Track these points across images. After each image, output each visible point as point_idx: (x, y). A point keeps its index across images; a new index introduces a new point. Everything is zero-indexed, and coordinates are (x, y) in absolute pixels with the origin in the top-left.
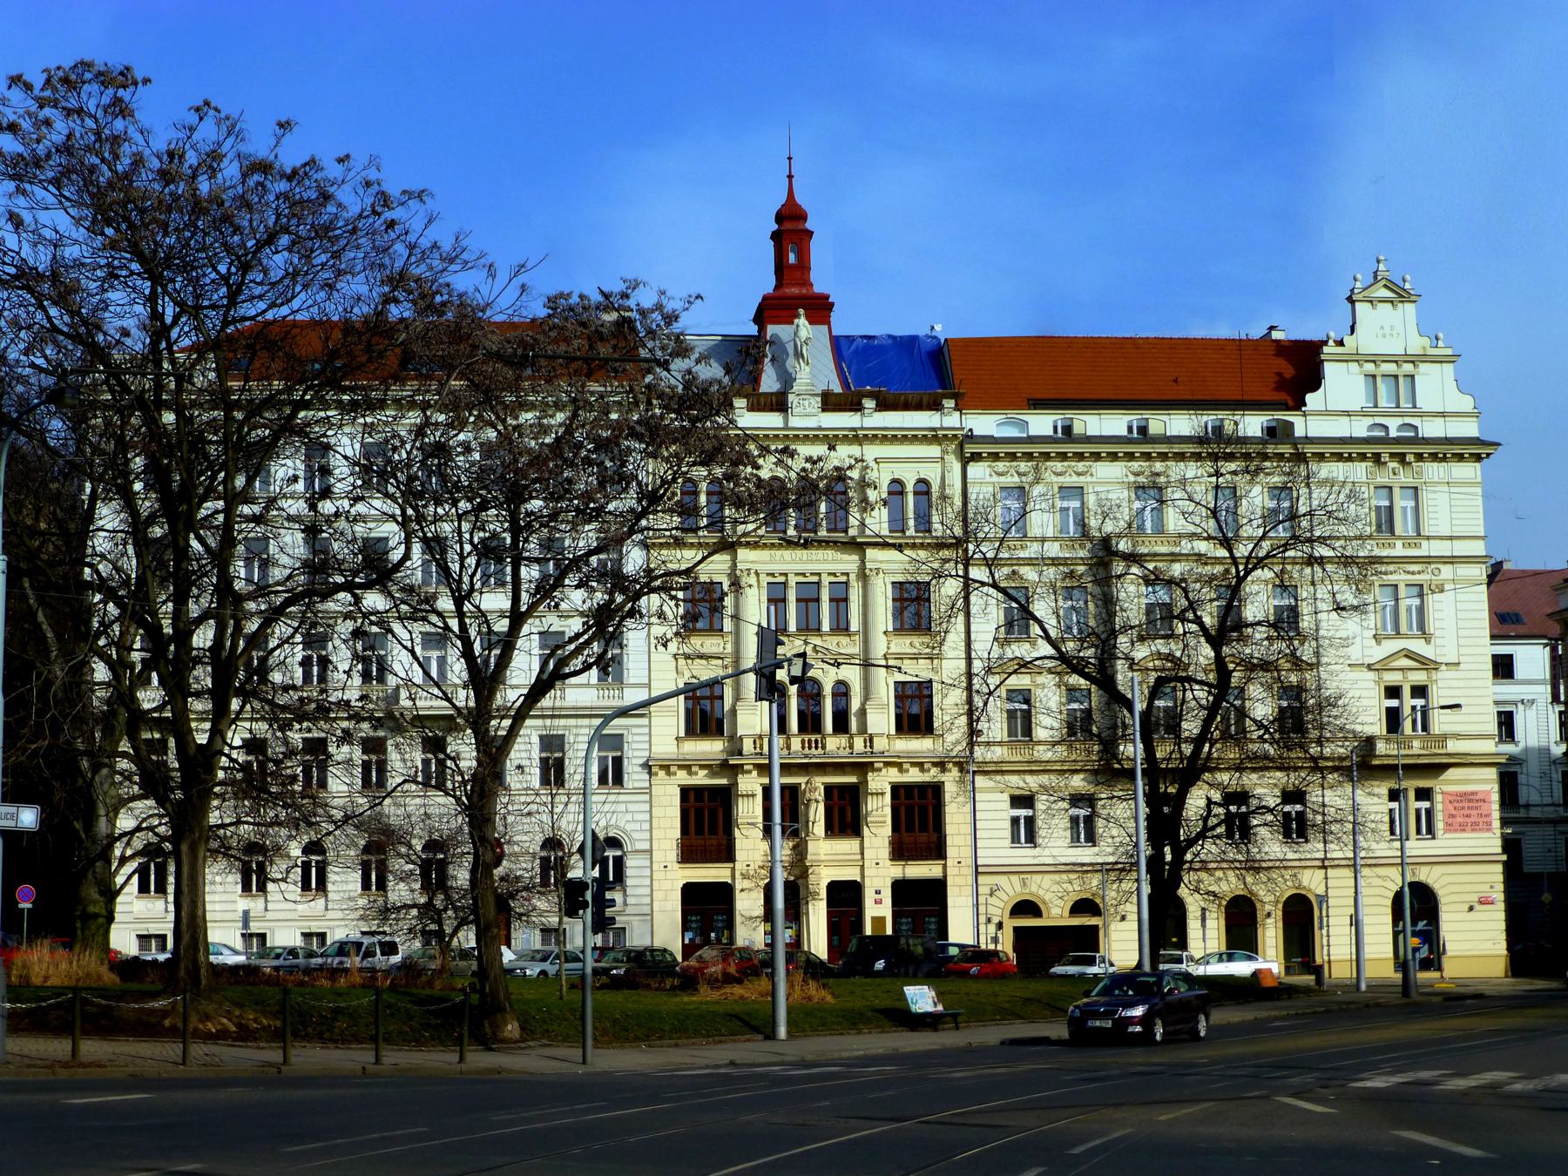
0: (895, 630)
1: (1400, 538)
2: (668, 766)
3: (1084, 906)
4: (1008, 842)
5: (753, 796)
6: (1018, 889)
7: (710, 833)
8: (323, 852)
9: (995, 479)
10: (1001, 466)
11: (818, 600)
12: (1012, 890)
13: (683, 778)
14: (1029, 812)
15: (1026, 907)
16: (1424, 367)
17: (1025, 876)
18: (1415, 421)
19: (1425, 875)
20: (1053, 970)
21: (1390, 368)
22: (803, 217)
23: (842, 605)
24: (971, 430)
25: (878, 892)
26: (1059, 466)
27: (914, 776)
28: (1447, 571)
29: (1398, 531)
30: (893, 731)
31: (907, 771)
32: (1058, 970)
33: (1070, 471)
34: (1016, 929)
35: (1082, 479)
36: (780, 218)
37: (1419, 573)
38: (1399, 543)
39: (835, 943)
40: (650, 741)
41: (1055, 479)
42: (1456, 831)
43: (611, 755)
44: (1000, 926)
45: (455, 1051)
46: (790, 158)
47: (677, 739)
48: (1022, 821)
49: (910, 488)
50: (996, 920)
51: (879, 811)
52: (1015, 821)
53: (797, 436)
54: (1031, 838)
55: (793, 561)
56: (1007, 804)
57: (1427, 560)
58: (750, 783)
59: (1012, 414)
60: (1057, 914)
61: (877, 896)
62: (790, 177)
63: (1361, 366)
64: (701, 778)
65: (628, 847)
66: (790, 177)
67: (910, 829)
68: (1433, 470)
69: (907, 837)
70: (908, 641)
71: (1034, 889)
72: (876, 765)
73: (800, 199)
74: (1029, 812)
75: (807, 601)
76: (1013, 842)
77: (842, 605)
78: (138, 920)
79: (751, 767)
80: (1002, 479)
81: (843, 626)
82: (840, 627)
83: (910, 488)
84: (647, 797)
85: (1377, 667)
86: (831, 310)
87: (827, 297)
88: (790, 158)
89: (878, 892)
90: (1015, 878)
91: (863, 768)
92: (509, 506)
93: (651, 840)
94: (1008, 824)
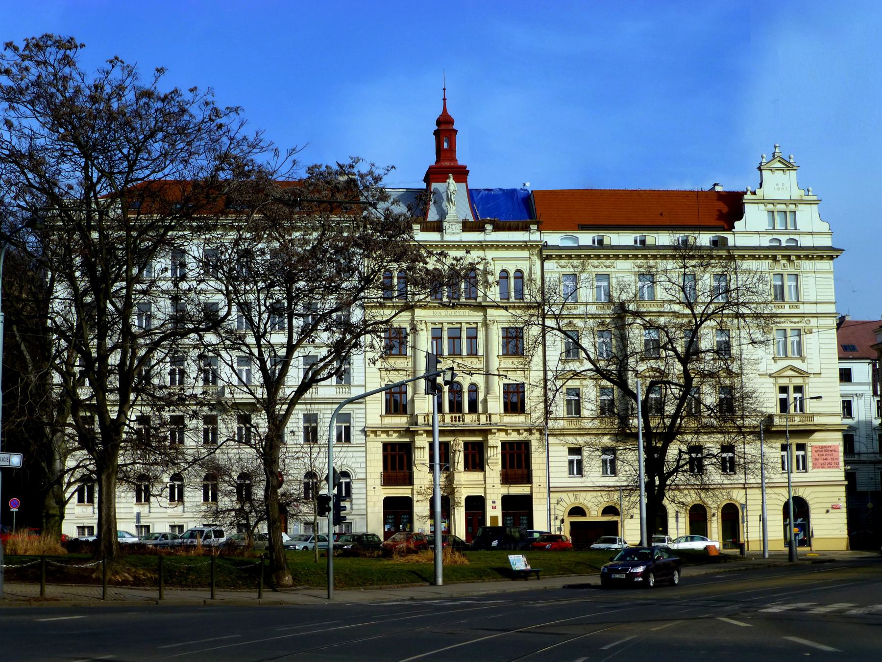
0: (503, 354)
1: (788, 303)
2: (376, 431)
3: (610, 510)
4: (567, 474)
5: (424, 448)
6: (573, 500)
7: (399, 469)
8: (181, 479)
9: (560, 269)
10: (563, 262)
11: (460, 338)
12: (569, 501)
13: (384, 438)
14: (579, 457)
15: (577, 511)
16: (801, 207)
17: (576, 493)
18: (796, 237)
19: (801, 493)
20: (592, 546)
21: (782, 207)
22: (452, 122)
23: (474, 340)
24: (546, 242)
25: (494, 502)
26: (596, 262)
27: (514, 437)
28: (814, 322)
29: (786, 299)
30: (502, 412)
31: (510, 434)
32: (595, 546)
33: (602, 265)
34: (571, 523)
35: (609, 269)
36: (438, 122)
37: (798, 322)
38: (787, 306)
39: (470, 531)
40: (366, 417)
41: (593, 269)
42: (819, 468)
43: (343, 425)
44: (562, 521)
45: (256, 592)
46: (444, 89)
47: (381, 416)
48: (575, 462)
49: (512, 274)
50: (560, 518)
51: (494, 456)
52: (571, 462)
53: (448, 245)
54: (580, 472)
55: (446, 316)
56: (567, 453)
57: (803, 315)
58: (422, 441)
59: (569, 233)
60: (594, 514)
61: (493, 505)
62: (444, 100)
63: (766, 206)
64: (394, 438)
65: (353, 477)
66: (444, 100)
67: (512, 466)
68: (806, 265)
69: (510, 471)
70: (511, 361)
71: (582, 500)
72: (493, 431)
73: (450, 112)
74: (579, 457)
75: (454, 338)
76: (570, 474)
77: (474, 340)
78: (78, 518)
79: (422, 432)
80: (564, 270)
81: (474, 352)
82: (473, 353)
83: (512, 274)
84: (364, 449)
85: (774, 375)
86: (467, 174)
87: (465, 167)
88: (444, 89)
89: (494, 502)
90: (571, 494)
91: (485, 432)
92: (286, 285)
93: (366, 473)
94: (567, 464)
